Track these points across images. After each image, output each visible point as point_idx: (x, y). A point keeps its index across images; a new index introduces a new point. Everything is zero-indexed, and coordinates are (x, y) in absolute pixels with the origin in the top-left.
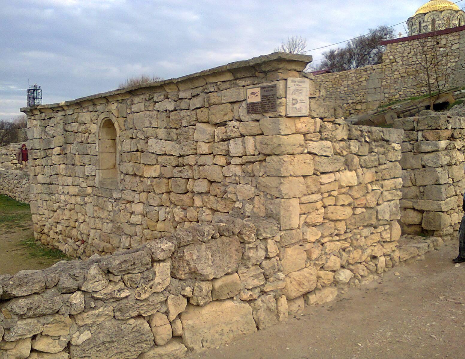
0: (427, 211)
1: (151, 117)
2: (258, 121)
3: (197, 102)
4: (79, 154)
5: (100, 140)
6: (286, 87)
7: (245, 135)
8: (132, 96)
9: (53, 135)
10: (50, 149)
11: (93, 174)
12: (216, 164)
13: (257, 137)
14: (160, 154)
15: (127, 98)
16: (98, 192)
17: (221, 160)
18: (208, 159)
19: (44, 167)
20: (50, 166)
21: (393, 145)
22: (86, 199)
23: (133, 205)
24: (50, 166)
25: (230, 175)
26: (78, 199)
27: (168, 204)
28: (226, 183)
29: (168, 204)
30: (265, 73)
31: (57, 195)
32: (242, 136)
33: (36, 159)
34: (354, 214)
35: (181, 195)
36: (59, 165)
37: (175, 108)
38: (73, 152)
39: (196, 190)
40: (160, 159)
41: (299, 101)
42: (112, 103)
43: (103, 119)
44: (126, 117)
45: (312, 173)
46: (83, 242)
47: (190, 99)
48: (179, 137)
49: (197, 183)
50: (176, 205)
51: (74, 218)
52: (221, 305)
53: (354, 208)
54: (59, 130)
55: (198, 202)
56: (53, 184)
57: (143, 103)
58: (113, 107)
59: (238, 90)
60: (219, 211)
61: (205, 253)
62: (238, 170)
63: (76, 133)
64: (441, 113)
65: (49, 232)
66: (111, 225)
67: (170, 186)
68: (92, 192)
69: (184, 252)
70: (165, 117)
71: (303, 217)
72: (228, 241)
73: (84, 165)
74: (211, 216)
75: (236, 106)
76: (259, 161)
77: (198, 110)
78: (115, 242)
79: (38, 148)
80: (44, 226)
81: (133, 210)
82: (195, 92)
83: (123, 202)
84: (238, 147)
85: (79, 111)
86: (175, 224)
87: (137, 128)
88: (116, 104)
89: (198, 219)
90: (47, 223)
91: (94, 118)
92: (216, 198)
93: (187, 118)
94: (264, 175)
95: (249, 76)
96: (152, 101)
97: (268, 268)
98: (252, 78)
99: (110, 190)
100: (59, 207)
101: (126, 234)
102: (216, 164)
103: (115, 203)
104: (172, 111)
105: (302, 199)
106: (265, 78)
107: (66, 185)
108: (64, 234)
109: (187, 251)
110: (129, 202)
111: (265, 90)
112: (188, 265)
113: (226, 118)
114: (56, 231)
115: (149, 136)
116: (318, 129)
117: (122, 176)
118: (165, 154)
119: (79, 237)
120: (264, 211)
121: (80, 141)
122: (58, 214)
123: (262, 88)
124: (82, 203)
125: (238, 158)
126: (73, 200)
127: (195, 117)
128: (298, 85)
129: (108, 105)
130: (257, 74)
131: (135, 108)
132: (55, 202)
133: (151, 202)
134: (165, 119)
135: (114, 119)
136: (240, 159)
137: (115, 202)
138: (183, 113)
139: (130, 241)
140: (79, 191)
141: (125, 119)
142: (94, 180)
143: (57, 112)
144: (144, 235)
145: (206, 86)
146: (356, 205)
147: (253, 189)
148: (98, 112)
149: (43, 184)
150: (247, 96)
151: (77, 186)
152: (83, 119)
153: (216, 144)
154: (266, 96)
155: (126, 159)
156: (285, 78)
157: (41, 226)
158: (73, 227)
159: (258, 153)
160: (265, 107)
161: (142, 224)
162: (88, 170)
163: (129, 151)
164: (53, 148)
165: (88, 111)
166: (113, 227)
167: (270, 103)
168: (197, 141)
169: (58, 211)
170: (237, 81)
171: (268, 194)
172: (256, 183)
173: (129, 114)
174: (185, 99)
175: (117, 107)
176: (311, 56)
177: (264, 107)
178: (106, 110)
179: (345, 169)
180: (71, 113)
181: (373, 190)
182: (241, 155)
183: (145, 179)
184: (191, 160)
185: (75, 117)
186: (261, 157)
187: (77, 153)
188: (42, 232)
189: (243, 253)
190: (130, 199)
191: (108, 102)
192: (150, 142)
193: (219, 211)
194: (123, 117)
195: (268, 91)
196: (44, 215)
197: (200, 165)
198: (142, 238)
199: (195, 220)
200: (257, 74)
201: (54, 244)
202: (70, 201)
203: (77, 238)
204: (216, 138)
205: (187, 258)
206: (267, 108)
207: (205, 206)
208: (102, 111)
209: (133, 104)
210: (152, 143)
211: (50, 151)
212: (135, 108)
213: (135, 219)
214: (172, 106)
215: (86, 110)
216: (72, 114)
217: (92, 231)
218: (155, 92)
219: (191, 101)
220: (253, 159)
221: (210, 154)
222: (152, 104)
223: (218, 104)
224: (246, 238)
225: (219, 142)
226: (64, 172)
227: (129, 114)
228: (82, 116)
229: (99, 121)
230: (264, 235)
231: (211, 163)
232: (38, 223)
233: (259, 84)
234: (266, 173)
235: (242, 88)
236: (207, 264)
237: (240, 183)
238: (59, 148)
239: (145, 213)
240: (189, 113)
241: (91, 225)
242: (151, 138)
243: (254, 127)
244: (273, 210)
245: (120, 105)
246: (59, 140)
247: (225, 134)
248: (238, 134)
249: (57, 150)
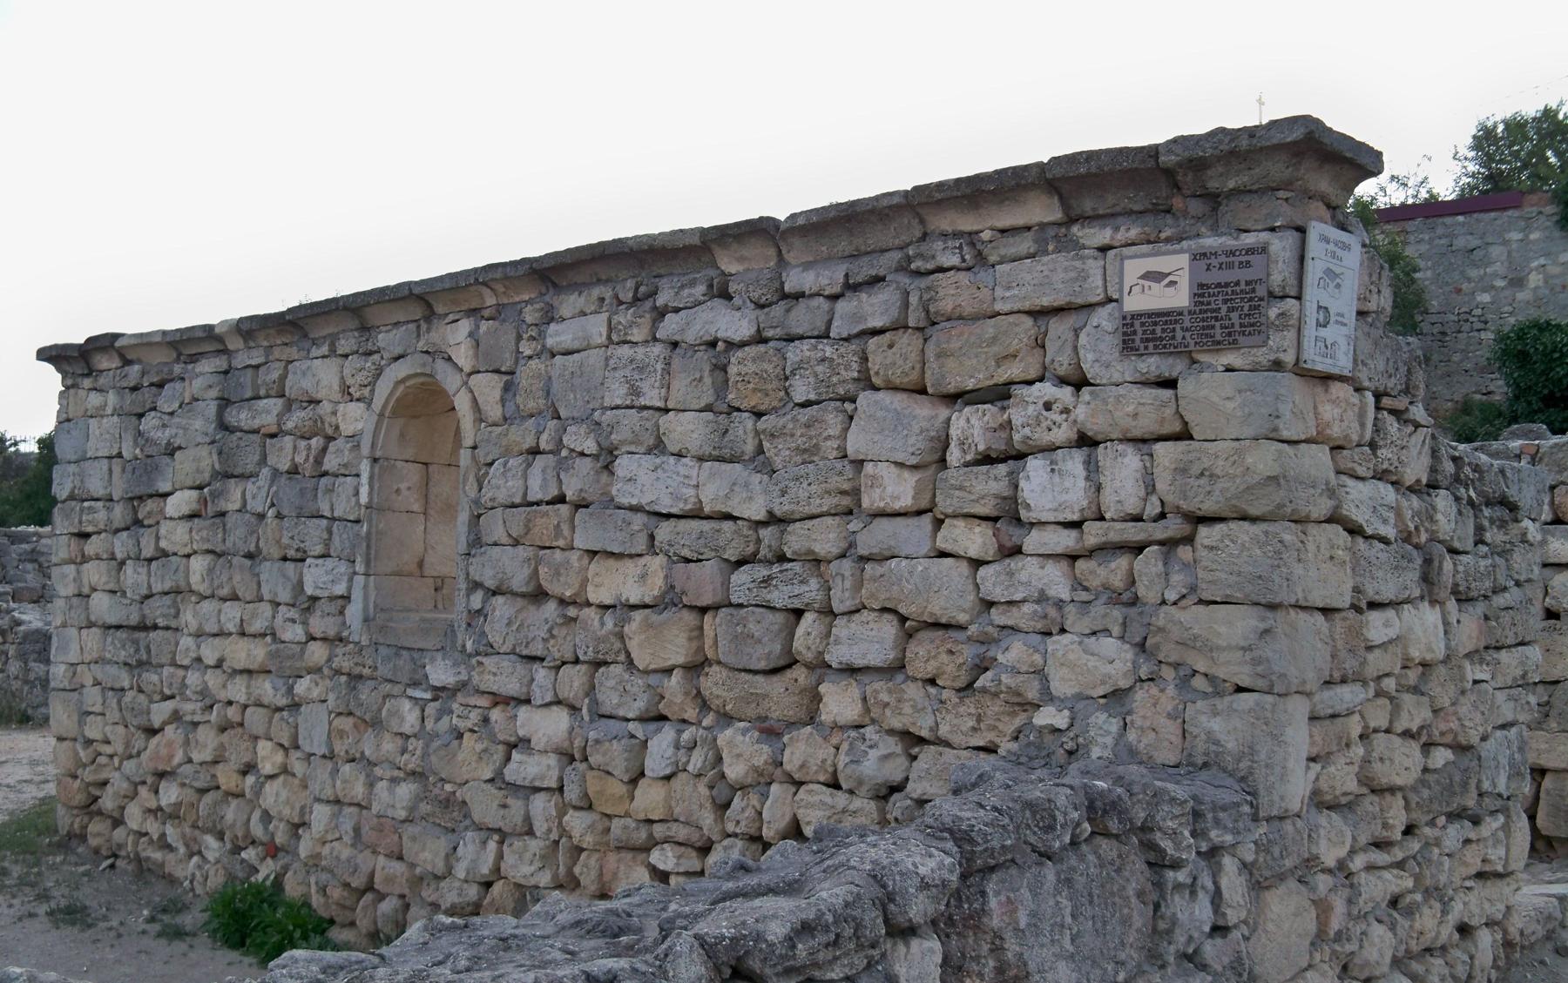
0: (1556, 771)
1: (641, 369)
2: (1170, 384)
3: (875, 308)
4: (279, 516)
5: (375, 460)
6: (1302, 259)
7: (1099, 438)
8: (551, 291)
9: (169, 443)
10: (151, 496)
11: (340, 589)
12: (943, 554)
13: (1159, 448)
14: (674, 511)
15: (526, 297)
16: (359, 660)
17: (974, 540)
18: (915, 534)
19: (123, 563)
20: (150, 560)
21: (1527, 523)
22: (302, 687)
23: (523, 712)
24: (150, 560)
25: (1018, 597)
26: (267, 689)
27: (691, 713)
28: (990, 629)
29: (691, 713)
30: (1214, 200)
31: (167, 671)
32: (1085, 441)
33: (85, 536)
34: (1425, 770)
35: (760, 679)
36: (188, 556)
37: (759, 331)
38: (257, 505)
39: (837, 655)
40: (664, 531)
41: (1333, 319)
42: (451, 317)
43: (403, 381)
44: (512, 373)
45: (303, 709)
46: (272, 851)
47: (834, 298)
48: (766, 445)
50: (727, 718)
51: (237, 755)
53: (1427, 747)
54: (198, 424)
55: (840, 702)
56: (155, 627)
57: (605, 316)
58: (457, 336)
59: (1078, 264)
60: (948, 744)
61: (1051, 902)
62: (1056, 581)
63: (273, 436)
65: (123, 808)
66: (406, 790)
67: (708, 642)
68: (329, 660)
69: (983, 893)
70: (707, 368)
71: (1316, 767)
72: (1114, 854)
73: (299, 555)
74: (902, 761)
75: (1058, 329)
76: (1161, 543)
77: (873, 342)
78: (429, 854)
79: (101, 492)
80: (105, 783)
81: (521, 733)
82: (864, 270)
83: (473, 701)
84: (1067, 484)
85: (293, 352)
86: (722, 792)
87: (563, 414)
88: (465, 326)
89: (835, 773)
90: (117, 775)
91: (361, 378)
92: (932, 690)
93: (820, 369)
94: (1184, 596)
95: (1136, 208)
96: (648, 304)
97: (1220, 969)
98: (1150, 218)
99: (416, 655)
100: (176, 717)
101: (479, 828)
102: (943, 554)
103: (437, 704)
104: (742, 344)
105: (1317, 698)
106: (1210, 222)
107: (215, 631)
108: (191, 818)
109: (997, 893)
110: (499, 700)
111: (1215, 262)
112: (997, 950)
113: (1014, 371)
114: (153, 805)
115: (623, 442)
116: (1368, 436)
117: (476, 600)
118: (697, 514)
119: (257, 830)
120: (1177, 740)
121: (284, 465)
122: (170, 744)
123: (1197, 257)
124: (283, 702)
125: (1060, 529)
126: (238, 690)
128: (1334, 255)
129: (428, 330)
130: (1177, 202)
131: (557, 334)
132: (157, 697)
133: (609, 699)
134: (706, 374)
135: (450, 381)
136: (1074, 533)
137: (434, 699)
138: (795, 352)
139: (500, 856)
140: (272, 655)
141: (508, 377)
142: (342, 613)
143: (194, 359)
144: (564, 832)
145: (924, 247)
146: (1437, 738)
147: (1128, 654)
148: (376, 357)
149: (110, 627)
150: (1121, 283)
151: (264, 635)
152: (307, 384)
154: (1219, 285)
155: (499, 533)
156: (1299, 223)
157: (89, 784)
158: (228, 794)
159: (1158, 510)
160: (1213, 327)
161: (561, 789)
162: (315, 577)
163: (518, 500)
164: (166, 495)
165: (333, 352)
166: (419, 798)
167: (1234, 316)
169: (169, 729)
170: (1075, 229)
171: (1195, 672)
172: (1142, 632)
173: (530, 357)
174: (812, 296)
175: (471, 335)
177: (1203, 328)
178: (421, 345)
179: (1422, 598)
180: (253, 362)
181: (1476, 682)
182: (1076, 517)
183: (587, 610)
184: (824, 538)
185: (275, 375)
186: (1173, 527)
187: (271, 513)
188: (93, 807)
189: (1157, 907)
190: (512, 687)
191: (430, 316)
192: (623, 465)
193: (948, 744)
194: (497, 371)
195: (1230, 266)
196: (108, 742)
198: (556, 843)
199: (822, 779)
200: (1177, 202)
201: (143, 855)
202: (223, 695)
203: (247, 833)
205: (995, 922)
206: (1218, 333)
207: (873, 721)
208: (398, 350)
209: (552, 320)
210: (634, 467)
211: (150, 505)
212: (559, 336)
213: (524, 768)
214: (745, 323)
215: (325, 349)
216: (257, 367)
217: (320, 815)
218: (662, 271)
219: (841, 306)
220: (1133, 532)
221: (919, 513)
222: (647, 319)
223: (976, 318)
224: (1166, 844)
226: (206, 585)
227: (530, 357)
228: (304, 374)
229: (383, 388)
230: (1213, 834)
231: (925, 550)
232: (79, 772)
233: (1181, 240)
234: (1193, 589)
235: (1096, 253)
236: (1057, 949)
237: (1063, 631)
238: (195, 493)
239: (578, 743)
240: (829, 351)
241: (315, 787)
242: (633, 448)
243: (1147, 411)
244: (1222, 737)
245: (484, 326)
246: (197, 461)
247: (1004, 435)
248: (1063, 434)
249: (180, 502)
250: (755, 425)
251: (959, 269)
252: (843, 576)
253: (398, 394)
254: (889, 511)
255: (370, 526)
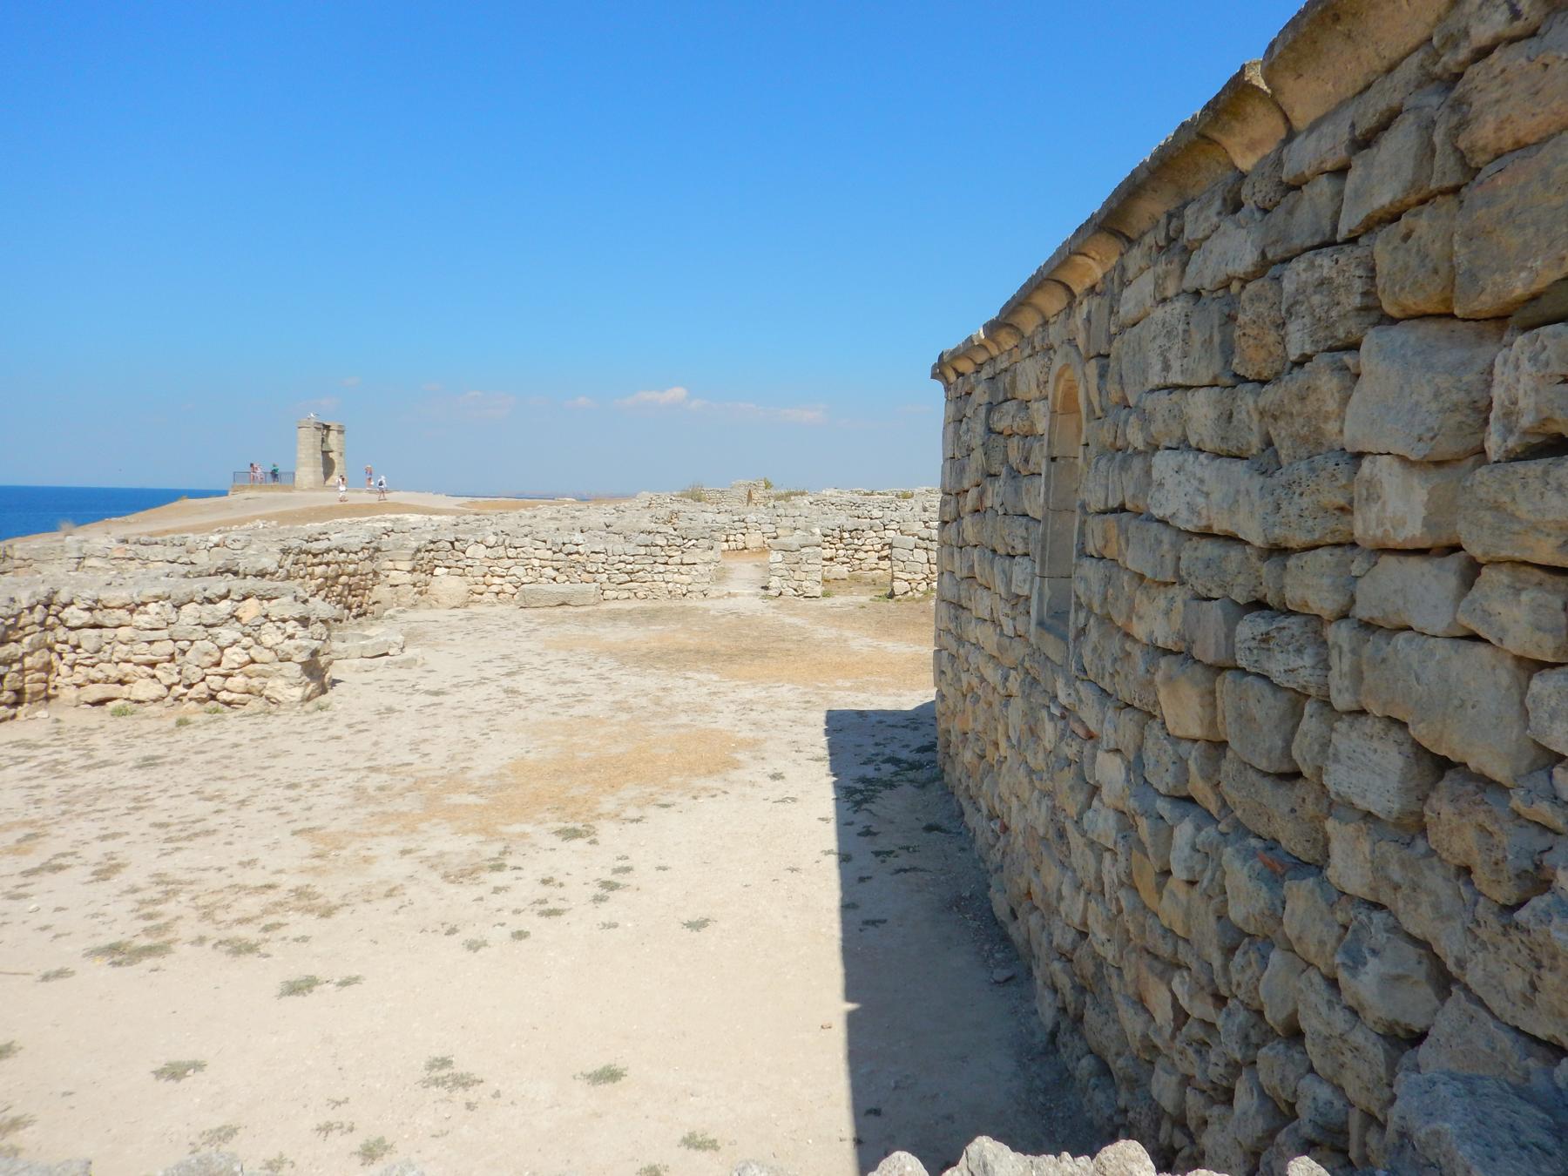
5: (1053, 459)
37: (1263, 254)
49: (1346, 738)
52: (1417, 1051)
64: (378, 517)
127: (1358, 285)
153: (1484, 482)
168: (1359, 456)
176: (932, 378)
197: (1368, 626)
204: (1494, 427)
225: (1514, 457)
231: (1439, 624)
250: (1256, 402)
251: (1512, 40)
252: (1340, 647)
253: (1061, 388)
254: (1391, 545)
255: (1046, 528)
